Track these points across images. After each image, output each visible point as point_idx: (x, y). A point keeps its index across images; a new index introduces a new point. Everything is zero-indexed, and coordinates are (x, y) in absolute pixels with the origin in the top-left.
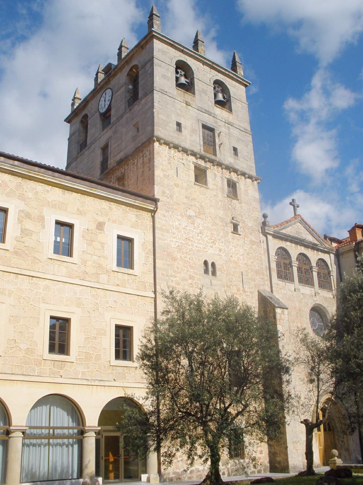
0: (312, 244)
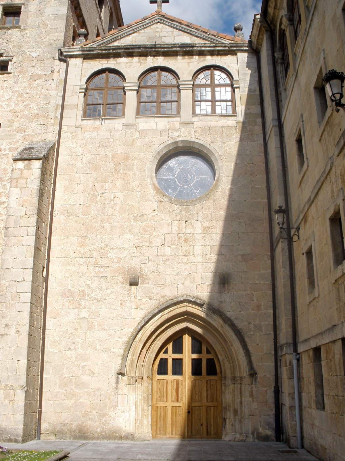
0: (180, 47)
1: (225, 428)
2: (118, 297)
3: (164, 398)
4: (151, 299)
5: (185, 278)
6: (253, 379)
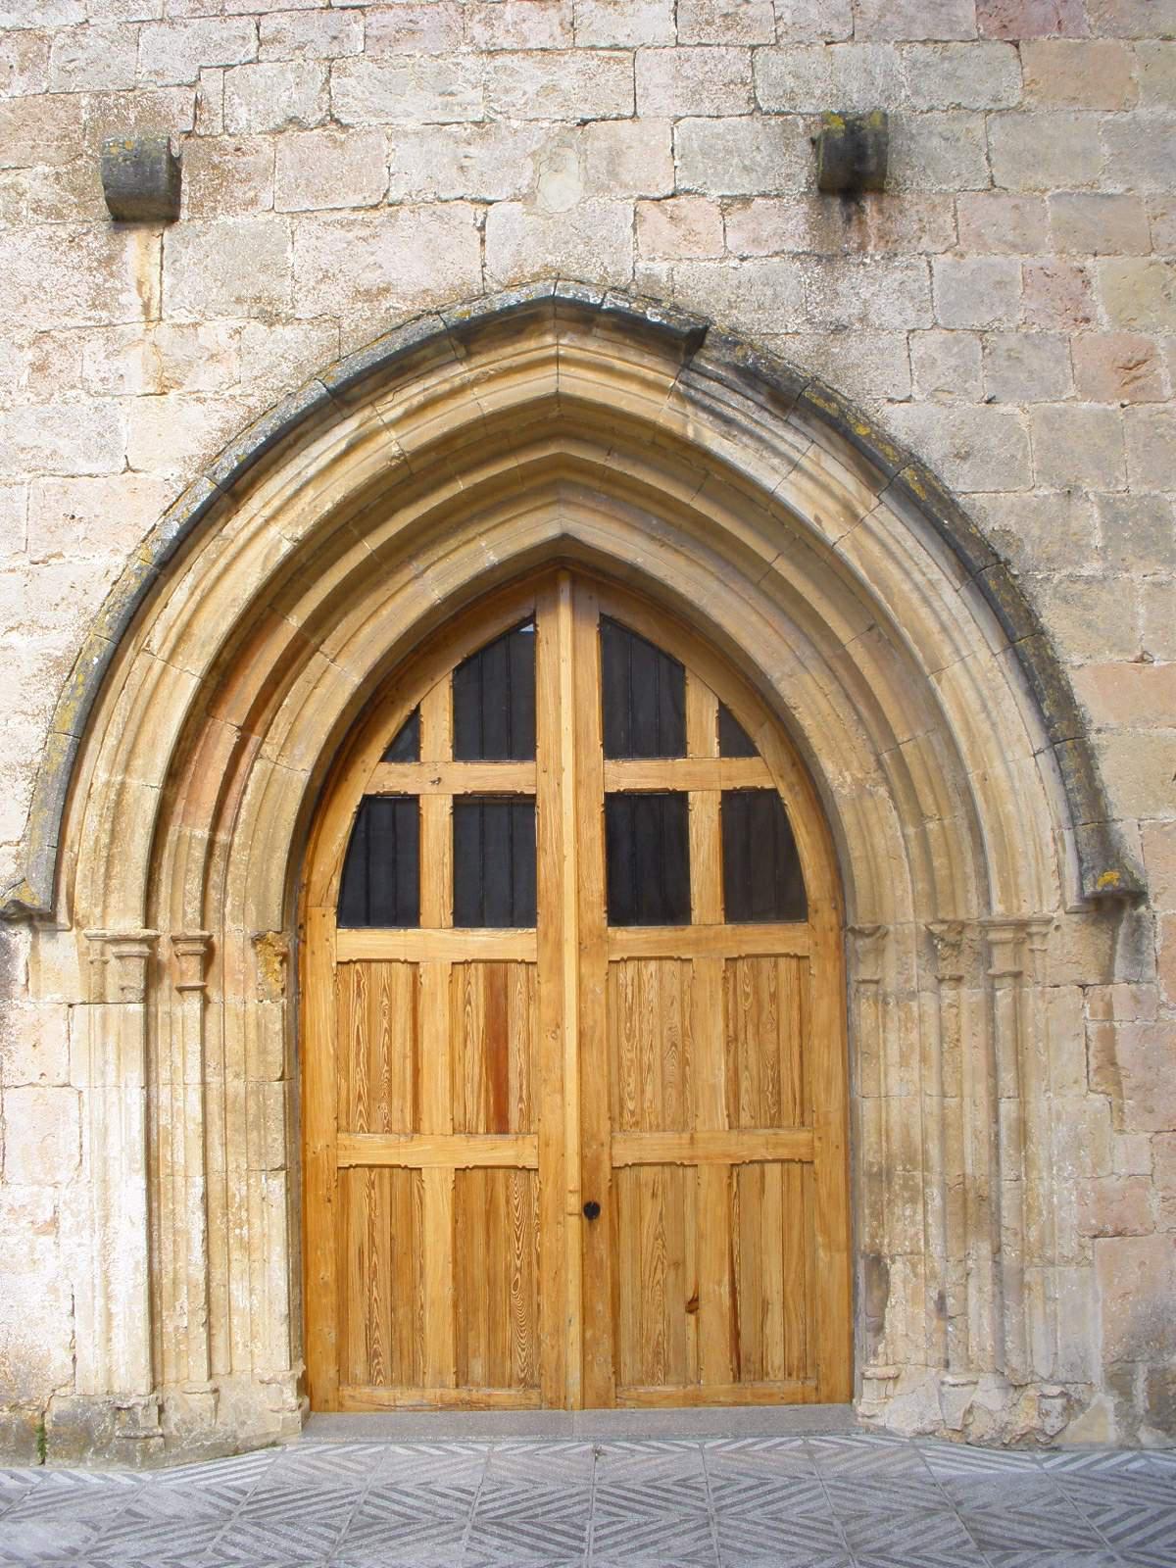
1: (879, 1329)
2: (18, 318)
3: (396, 1102)
4: (270, 319)
5: (549, 158)
6: (1114, 940)
